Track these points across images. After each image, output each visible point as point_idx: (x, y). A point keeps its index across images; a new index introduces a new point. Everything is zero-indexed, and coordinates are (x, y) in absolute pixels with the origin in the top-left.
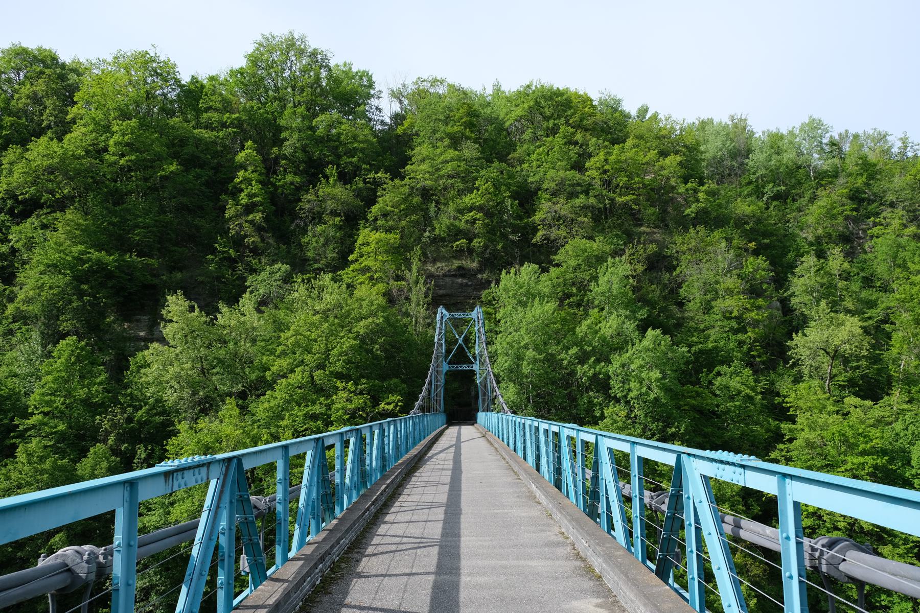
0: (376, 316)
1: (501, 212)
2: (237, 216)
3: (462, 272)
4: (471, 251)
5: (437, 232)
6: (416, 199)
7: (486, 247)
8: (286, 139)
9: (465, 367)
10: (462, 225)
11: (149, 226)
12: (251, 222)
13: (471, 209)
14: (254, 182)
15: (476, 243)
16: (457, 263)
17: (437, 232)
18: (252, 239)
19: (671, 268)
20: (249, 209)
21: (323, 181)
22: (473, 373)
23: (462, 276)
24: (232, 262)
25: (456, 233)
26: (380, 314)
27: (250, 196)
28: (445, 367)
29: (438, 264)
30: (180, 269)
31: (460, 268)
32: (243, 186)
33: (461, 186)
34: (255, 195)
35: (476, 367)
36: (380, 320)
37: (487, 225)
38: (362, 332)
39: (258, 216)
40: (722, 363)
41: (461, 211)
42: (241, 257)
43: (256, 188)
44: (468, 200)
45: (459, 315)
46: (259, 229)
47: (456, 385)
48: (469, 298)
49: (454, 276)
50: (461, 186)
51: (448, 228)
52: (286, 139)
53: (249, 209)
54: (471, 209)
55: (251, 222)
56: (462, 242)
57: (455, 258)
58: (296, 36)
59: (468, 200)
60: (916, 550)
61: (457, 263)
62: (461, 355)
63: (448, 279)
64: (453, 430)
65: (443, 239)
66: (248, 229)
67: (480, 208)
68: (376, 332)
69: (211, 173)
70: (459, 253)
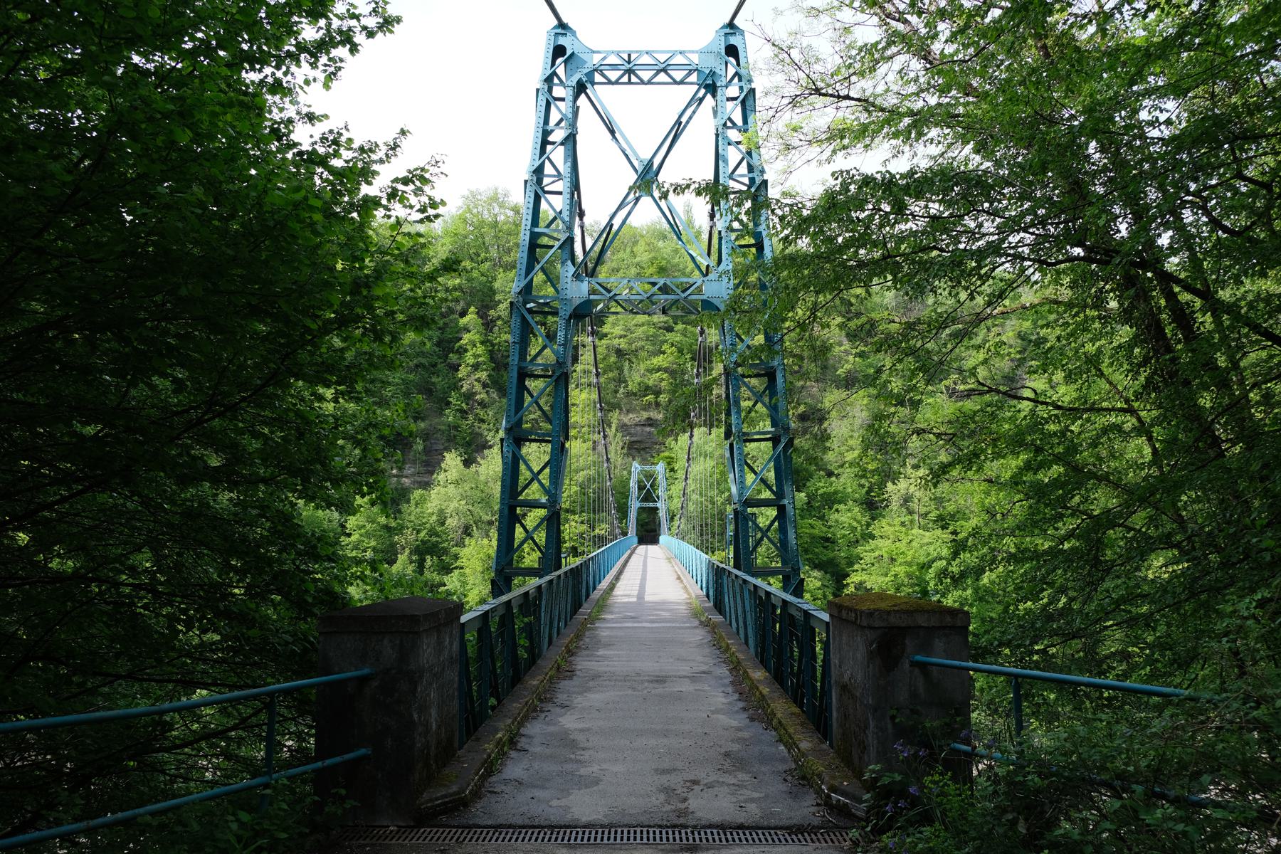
0: (589, 468)
1: (683, 373)
2: (469, 375)
3: (650, 422)
4: (657, 404)
5: (630, 388)
6: (613, 359)
7: (670, 401)
8: (500, 302)
9: (651, 505)
10: (651, 383)
11: (398, 384)
12: (478, 380)
13: (659, 369)
14: (478, 345)
15: (663, 398)
16: (645, 415)
17: (630, 388)
18: (482, 396)
19: (822, 420)
20: (476, 367)
21: (533, 340)
22: (657, 509)
23: (650, 425)
24: (463, 412)
25: (646, 389)
26: (592, 468)
27: (476, 356)
28: (638, 505)
29: (631, 416)
30: (423, 419)
31: (649, 419)
32: (469, 347)
33: (651, 348)
34: (479, 356)
35: (658, 505)
36: (592, 472)
37: (671, 384)
38: (581, 480)
39: (483, 375)
40: (840, 503)
41: (650, 371)
42: (472, 408)
43: (480, 349)
44: (658, 361)
45: (647, 468)
46: (485, 386)
47: (645, 515)
48: (656, 444)
49: (644, 425)
50: (651, 348)
51: (639, 384)
52: (500, 302)
53: (476, 367)
54: (659, 369)
55: (478, 380)
56: (651, 397)
57: (645, 410)
58: (500, 191)
59: (658, 361)
60: (116, 354)
61: (645, 415)
62: (648, 495)
63: (638, 428)
64: (642, 548)
65: (635, 394)
66: (478, 387)
67: (666, 370)
68: (590, 480)
69: (438, 333)
70: (646, 407)
